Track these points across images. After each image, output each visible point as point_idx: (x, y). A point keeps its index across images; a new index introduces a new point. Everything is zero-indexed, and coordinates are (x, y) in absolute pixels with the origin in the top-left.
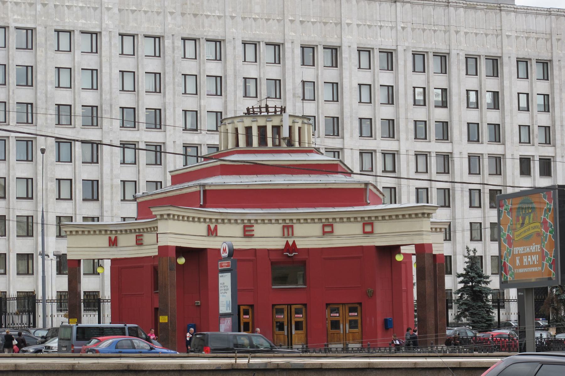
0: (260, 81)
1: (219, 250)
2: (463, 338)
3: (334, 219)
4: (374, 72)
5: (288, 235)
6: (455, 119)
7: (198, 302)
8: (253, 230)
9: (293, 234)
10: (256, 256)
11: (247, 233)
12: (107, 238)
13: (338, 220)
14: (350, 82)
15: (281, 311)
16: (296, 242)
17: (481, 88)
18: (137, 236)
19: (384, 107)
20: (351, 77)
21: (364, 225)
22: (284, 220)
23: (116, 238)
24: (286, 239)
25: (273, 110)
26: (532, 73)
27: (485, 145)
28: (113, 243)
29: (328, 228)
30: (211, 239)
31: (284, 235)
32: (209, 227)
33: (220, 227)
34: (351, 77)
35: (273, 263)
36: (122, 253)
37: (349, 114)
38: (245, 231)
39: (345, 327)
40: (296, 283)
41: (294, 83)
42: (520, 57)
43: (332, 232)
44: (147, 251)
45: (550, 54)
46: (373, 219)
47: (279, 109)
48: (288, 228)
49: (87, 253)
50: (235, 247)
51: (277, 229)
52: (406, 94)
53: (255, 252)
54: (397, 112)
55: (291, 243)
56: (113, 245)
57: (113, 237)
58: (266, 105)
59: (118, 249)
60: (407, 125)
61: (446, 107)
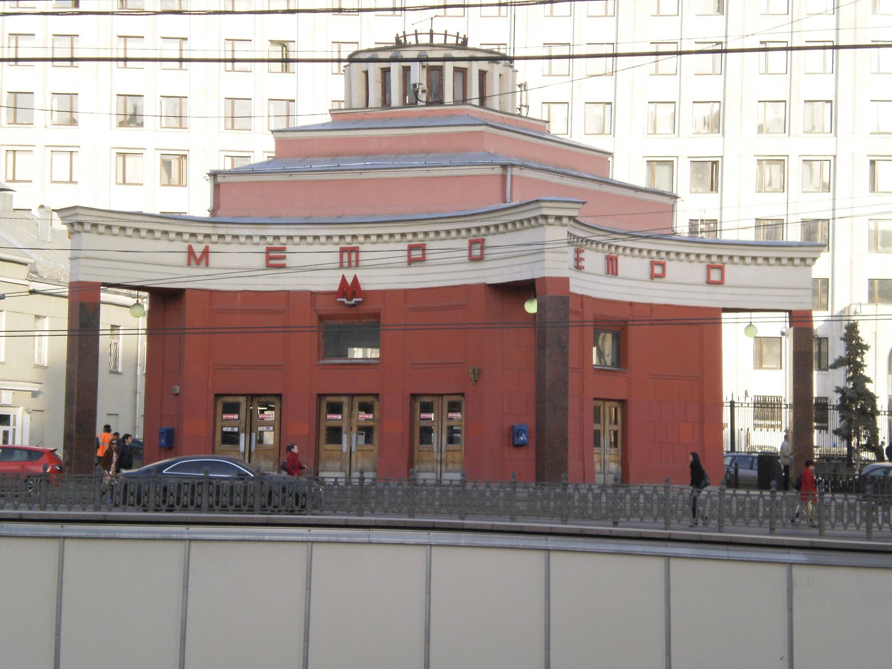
5: (350, 262)
7: (177, 389)
11: (272, 262)
15: (232, 408)
16: (359, 279)
22: (709, 256)
23: (206, 252)
29: (417, 255)
30: (611, 280)
32: (191, 252)
35: (321, 318)
38: (269, 258)
39: (438, 438)
46: (725, 260)
48: (350, 254)
53: (287, 295)
55: (350, 281)
56: (198, 262)
57: (198, 249)
58: (431, 31)
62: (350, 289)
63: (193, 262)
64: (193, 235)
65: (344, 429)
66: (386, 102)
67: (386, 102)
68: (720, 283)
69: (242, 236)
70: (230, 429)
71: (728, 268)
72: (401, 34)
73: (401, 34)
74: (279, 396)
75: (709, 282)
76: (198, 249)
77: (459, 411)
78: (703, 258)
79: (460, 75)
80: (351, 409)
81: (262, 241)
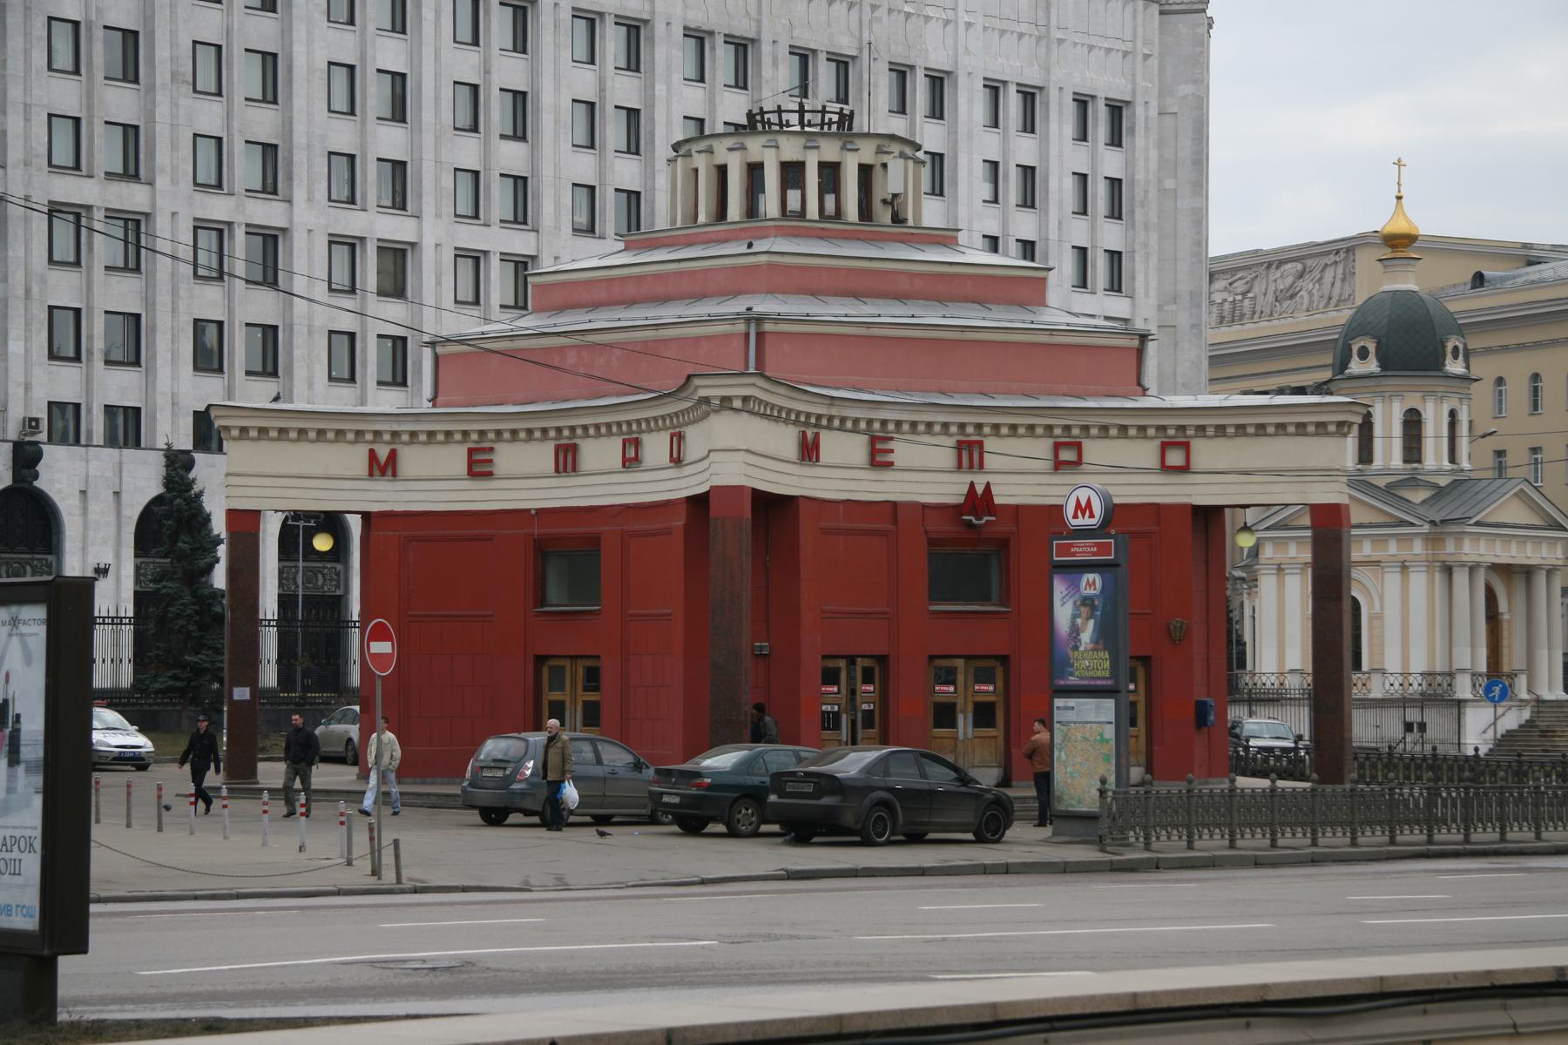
0: (89, 29)
1: (1059, 509)
2: (1413, 759)
3: (1085, 428)
4: (363, 33)
6: (547, 171)
8: (892, 451)
9: (981, 466)
10: (895, 520)
12: (362, 452)
13: (1094, 431)
14: (309, 53)
17: (602, 98)
18: (471, 451)
19: (383, 129)
20: (310, 42)
21: (1164, 447)
22: (962, 426)
23: (393, 455)
24: (968, 478)
25: (818, 119)
26: (714, 69)
27: (608, 241)
28: (383, 467)
30: (806, 470)
31: (960, 466)
32: (372, 454)
33: (825, 437)
34: (310, 42)
35: (932, 542)
36: (407, 496)
37: (304, 140)
38: (471, 462)
40: (986, 599)
41: (173, 44)
42: (693, 26)
43: (1079, 462)
44: (508, 495)
45: (754, 24)
47: (835, 118)
49: (294, 493)
50: (1116, 501)
51: (940, 453)
52: (437, 98)
53: (893, 509)
54: (415, 145)
55: (980, 489)
56: (383, 472)
57: (383, 453)
59: (399, 485)
60: (437, 179)
61: (524, 138)
62: (979, 501)
63: (376, 472)
64: (377, 434)
65: (959, 707)
66: (674, 221)
67: (674, 221)
68: (1185, 469)
69: (1171, 426)
70: (829, 708)
71: (1088, 445)
72: (756, 111)
73: (756, 111)
74: (1004, 659)
75: (1165, 468)
76: (383, 453)
77: (953, 682)
78: (1151, 432)
79: (398, 168)
80: (851, 678)
81: (1161, 434)
